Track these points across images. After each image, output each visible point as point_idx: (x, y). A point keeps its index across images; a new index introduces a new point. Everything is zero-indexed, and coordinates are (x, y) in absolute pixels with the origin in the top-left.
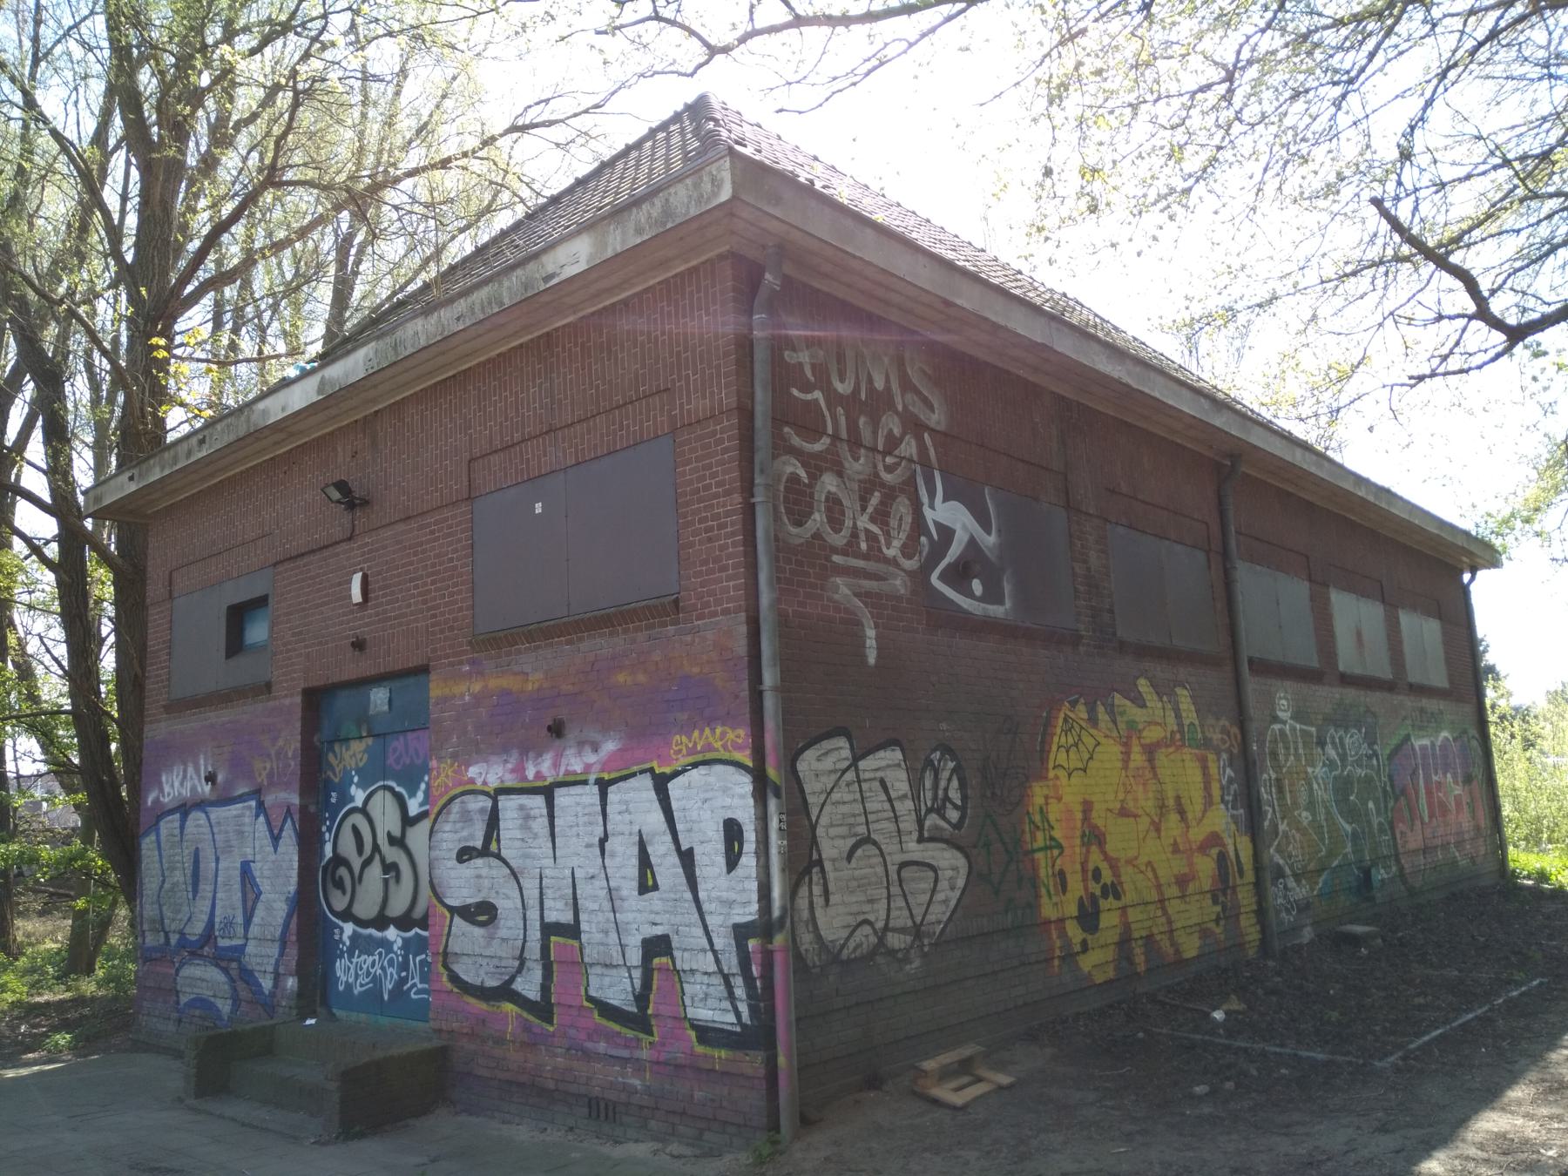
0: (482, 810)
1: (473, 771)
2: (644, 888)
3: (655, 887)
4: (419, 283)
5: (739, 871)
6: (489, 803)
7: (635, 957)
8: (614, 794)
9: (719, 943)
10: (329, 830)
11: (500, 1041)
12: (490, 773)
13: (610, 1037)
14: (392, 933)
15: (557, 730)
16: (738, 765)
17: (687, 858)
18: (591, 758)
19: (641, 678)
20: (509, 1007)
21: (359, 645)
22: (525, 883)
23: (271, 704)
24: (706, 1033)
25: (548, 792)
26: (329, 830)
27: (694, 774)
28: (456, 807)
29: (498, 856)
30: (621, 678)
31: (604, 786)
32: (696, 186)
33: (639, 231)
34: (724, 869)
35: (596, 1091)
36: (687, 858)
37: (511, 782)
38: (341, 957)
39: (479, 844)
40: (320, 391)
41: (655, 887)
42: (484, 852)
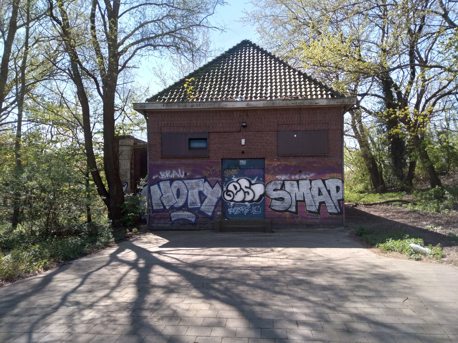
0: (280, 183)
1: (277, 177)
2: (319, 195)
3: (322, 195)
4: (108, 29)
5: (339, 193)
6: (282, 182)
7: (318, 204)
8: (313, 182)
9: (334, 202)
10: (225, 185)
11: (286, 218)
12: (283, 178)
13: (311, 215)
14: (247, 203)
15: (300, 172)
16: (339, 179)
17: (329, 191)
18: (308, 176)
19: (319, 165)
20: (287, 213)
21: (243, 152)
22: (291, 194)
23: (209, 160)
24: (331, 214)
25: (298, 181)
26: (225, 185)
27: (330, 180)
28: (273, 182)
29: (285, 190)
30: (315, 165)
31: (311, 181)
32: (350, 100)
33: (337, 102)
34: (336, 192)
35: (309, 223)
36: (329, 191)
37: (287, 179)
38: (230, 208)
39: (279, 188)
40: (247, 105)
41: (322, 195)
42: (281, 189)
